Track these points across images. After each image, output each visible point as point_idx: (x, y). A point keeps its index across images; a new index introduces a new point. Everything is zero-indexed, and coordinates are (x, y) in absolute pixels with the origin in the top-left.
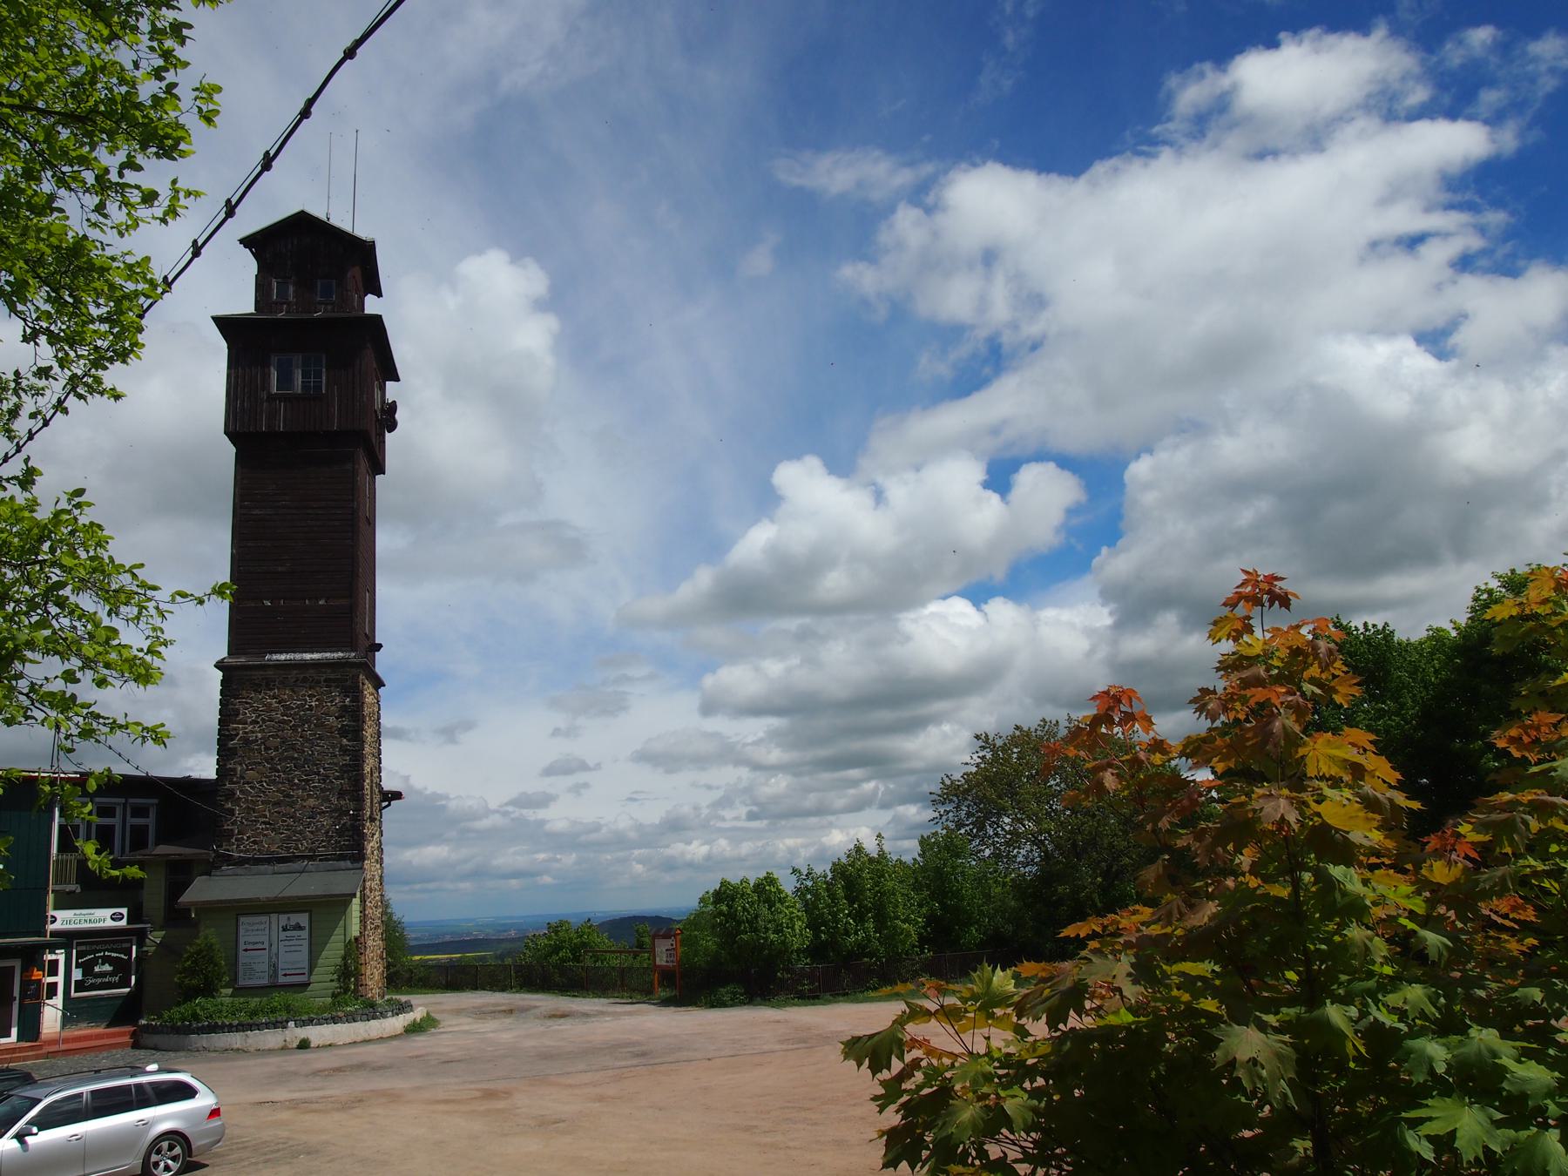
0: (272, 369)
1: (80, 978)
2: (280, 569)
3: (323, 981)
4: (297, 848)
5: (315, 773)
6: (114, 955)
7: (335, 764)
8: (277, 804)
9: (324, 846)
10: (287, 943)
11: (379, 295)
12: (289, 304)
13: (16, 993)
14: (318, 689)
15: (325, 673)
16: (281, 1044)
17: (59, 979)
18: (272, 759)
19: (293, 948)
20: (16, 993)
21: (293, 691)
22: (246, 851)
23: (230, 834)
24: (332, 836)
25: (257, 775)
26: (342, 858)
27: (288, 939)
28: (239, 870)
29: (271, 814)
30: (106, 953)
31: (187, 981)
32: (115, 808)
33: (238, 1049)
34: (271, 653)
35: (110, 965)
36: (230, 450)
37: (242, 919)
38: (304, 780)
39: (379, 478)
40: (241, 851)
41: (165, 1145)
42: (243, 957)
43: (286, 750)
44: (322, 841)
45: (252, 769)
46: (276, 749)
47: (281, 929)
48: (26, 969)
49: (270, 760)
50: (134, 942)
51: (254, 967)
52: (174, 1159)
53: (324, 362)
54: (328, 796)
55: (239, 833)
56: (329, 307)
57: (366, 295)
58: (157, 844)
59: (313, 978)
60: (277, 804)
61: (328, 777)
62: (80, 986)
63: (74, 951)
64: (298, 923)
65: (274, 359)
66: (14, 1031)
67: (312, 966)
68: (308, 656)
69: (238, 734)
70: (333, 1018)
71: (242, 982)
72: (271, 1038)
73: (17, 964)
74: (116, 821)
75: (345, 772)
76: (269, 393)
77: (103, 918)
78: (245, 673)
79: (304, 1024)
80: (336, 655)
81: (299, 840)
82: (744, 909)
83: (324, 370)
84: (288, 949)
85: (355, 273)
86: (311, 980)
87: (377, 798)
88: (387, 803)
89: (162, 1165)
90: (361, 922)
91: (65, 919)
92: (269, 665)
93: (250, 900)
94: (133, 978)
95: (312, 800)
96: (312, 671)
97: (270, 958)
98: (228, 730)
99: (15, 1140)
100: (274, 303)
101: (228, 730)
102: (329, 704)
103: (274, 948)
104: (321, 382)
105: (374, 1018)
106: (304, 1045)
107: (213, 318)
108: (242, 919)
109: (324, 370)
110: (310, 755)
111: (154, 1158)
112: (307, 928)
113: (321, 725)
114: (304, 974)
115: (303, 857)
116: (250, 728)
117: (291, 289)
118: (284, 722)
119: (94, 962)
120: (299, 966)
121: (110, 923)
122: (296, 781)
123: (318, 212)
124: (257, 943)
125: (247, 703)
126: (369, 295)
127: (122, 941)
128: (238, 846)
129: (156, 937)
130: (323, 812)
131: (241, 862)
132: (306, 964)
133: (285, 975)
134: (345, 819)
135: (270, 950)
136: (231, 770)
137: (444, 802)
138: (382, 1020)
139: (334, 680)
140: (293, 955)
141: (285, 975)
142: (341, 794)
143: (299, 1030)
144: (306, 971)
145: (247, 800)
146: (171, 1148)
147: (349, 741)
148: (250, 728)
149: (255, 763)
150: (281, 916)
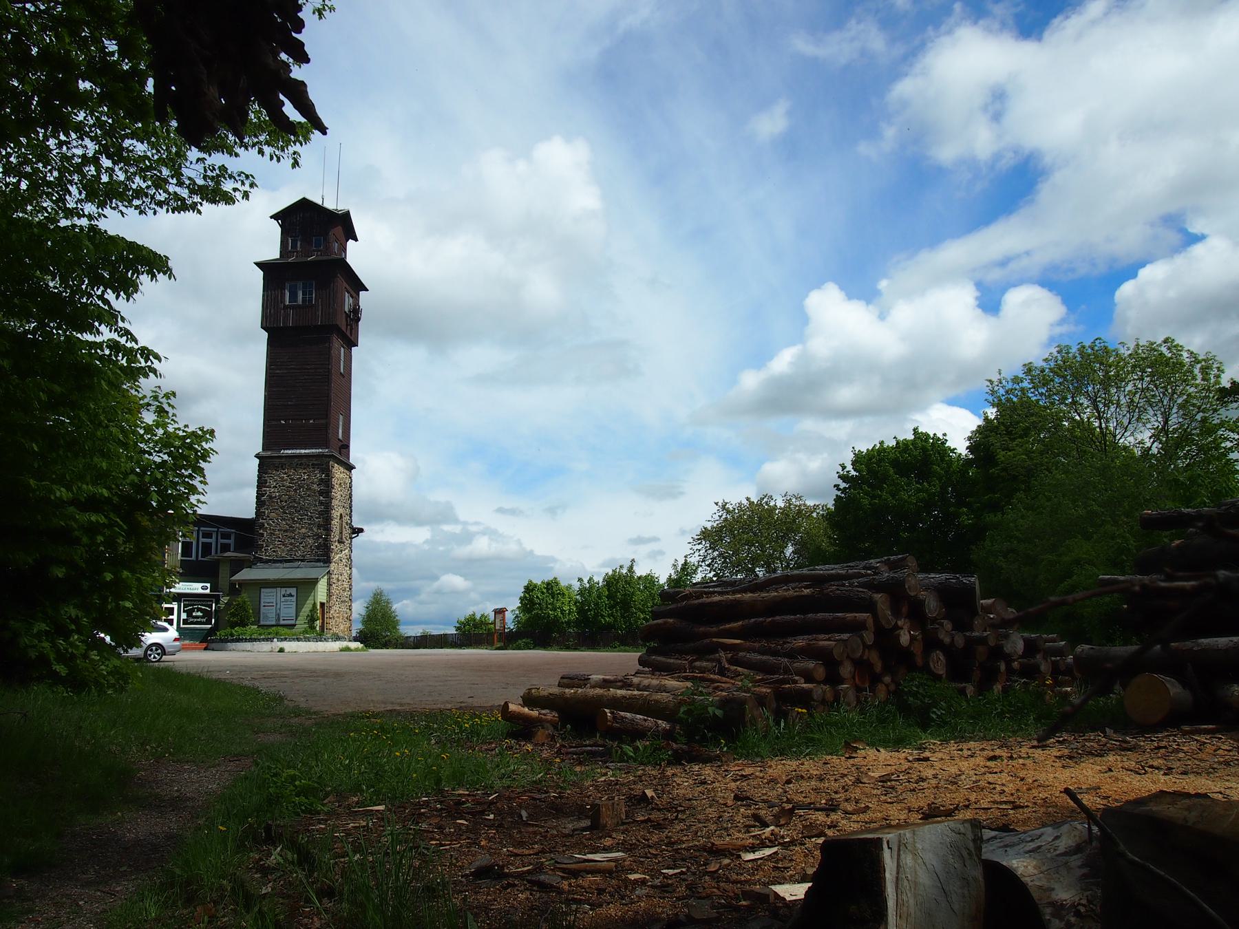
0: (286, 291)
1: (185, 618)
2: (289, 403)
3: (301, 624)
6: (204, 607)
8: (286, 531)
10: (285, 603)
11: (356, 240)
12: (297, 252)
17: (175, 617)
18: (284, 507)
21: (295, 470)
25: (276, 515)
26: (318, 561)
27: (286, 601)
28: (266, 566)
32: (212, 534)
37: (262, 590)
40: (267, 556)
41: (154, 648)
46: (286, 502)
51: (268, 615)
52: (158, 654)
56: (319, 253)
57: (347, 241)
59: (297, 622)
60: (286, 531)
62: (185, 622)
63: (182, 604)
65: (287, 285)
67: (297, 616)
70: (297, 639)
71: (262, 623)
76: (284, 304)
77: (197, 588)
82: (537, 597)
83: (314, 291)
84: (285, 606)
85: (339, 231)
87: (346, 532)
89: (153, 656)
91: (182, 587)
93: (266, 580)
94: (213, 620)
100: (290, 252)
103: (278, 606)
106: (282, 650)
108: (262, 590)
109: (314, 291)
111: (149, 652)
113: (309, 489)
115: (299, 560)
118: (290, 487)
119: (193, 610)
121: (201, 591)
122: (296, 519)
127: (208, 601)
129: (225, 600)
131: (267, 561)
132: (294, 615)
134: (321, 540)
137: (552, 565)
139: (316, 465)
140: (288, 611)
142: (319, 527)
143: (279, 643)
144: (294, 618)
145: (270, 529)
146: (156, 650)
149: (275, 509)
150: (282, 589)
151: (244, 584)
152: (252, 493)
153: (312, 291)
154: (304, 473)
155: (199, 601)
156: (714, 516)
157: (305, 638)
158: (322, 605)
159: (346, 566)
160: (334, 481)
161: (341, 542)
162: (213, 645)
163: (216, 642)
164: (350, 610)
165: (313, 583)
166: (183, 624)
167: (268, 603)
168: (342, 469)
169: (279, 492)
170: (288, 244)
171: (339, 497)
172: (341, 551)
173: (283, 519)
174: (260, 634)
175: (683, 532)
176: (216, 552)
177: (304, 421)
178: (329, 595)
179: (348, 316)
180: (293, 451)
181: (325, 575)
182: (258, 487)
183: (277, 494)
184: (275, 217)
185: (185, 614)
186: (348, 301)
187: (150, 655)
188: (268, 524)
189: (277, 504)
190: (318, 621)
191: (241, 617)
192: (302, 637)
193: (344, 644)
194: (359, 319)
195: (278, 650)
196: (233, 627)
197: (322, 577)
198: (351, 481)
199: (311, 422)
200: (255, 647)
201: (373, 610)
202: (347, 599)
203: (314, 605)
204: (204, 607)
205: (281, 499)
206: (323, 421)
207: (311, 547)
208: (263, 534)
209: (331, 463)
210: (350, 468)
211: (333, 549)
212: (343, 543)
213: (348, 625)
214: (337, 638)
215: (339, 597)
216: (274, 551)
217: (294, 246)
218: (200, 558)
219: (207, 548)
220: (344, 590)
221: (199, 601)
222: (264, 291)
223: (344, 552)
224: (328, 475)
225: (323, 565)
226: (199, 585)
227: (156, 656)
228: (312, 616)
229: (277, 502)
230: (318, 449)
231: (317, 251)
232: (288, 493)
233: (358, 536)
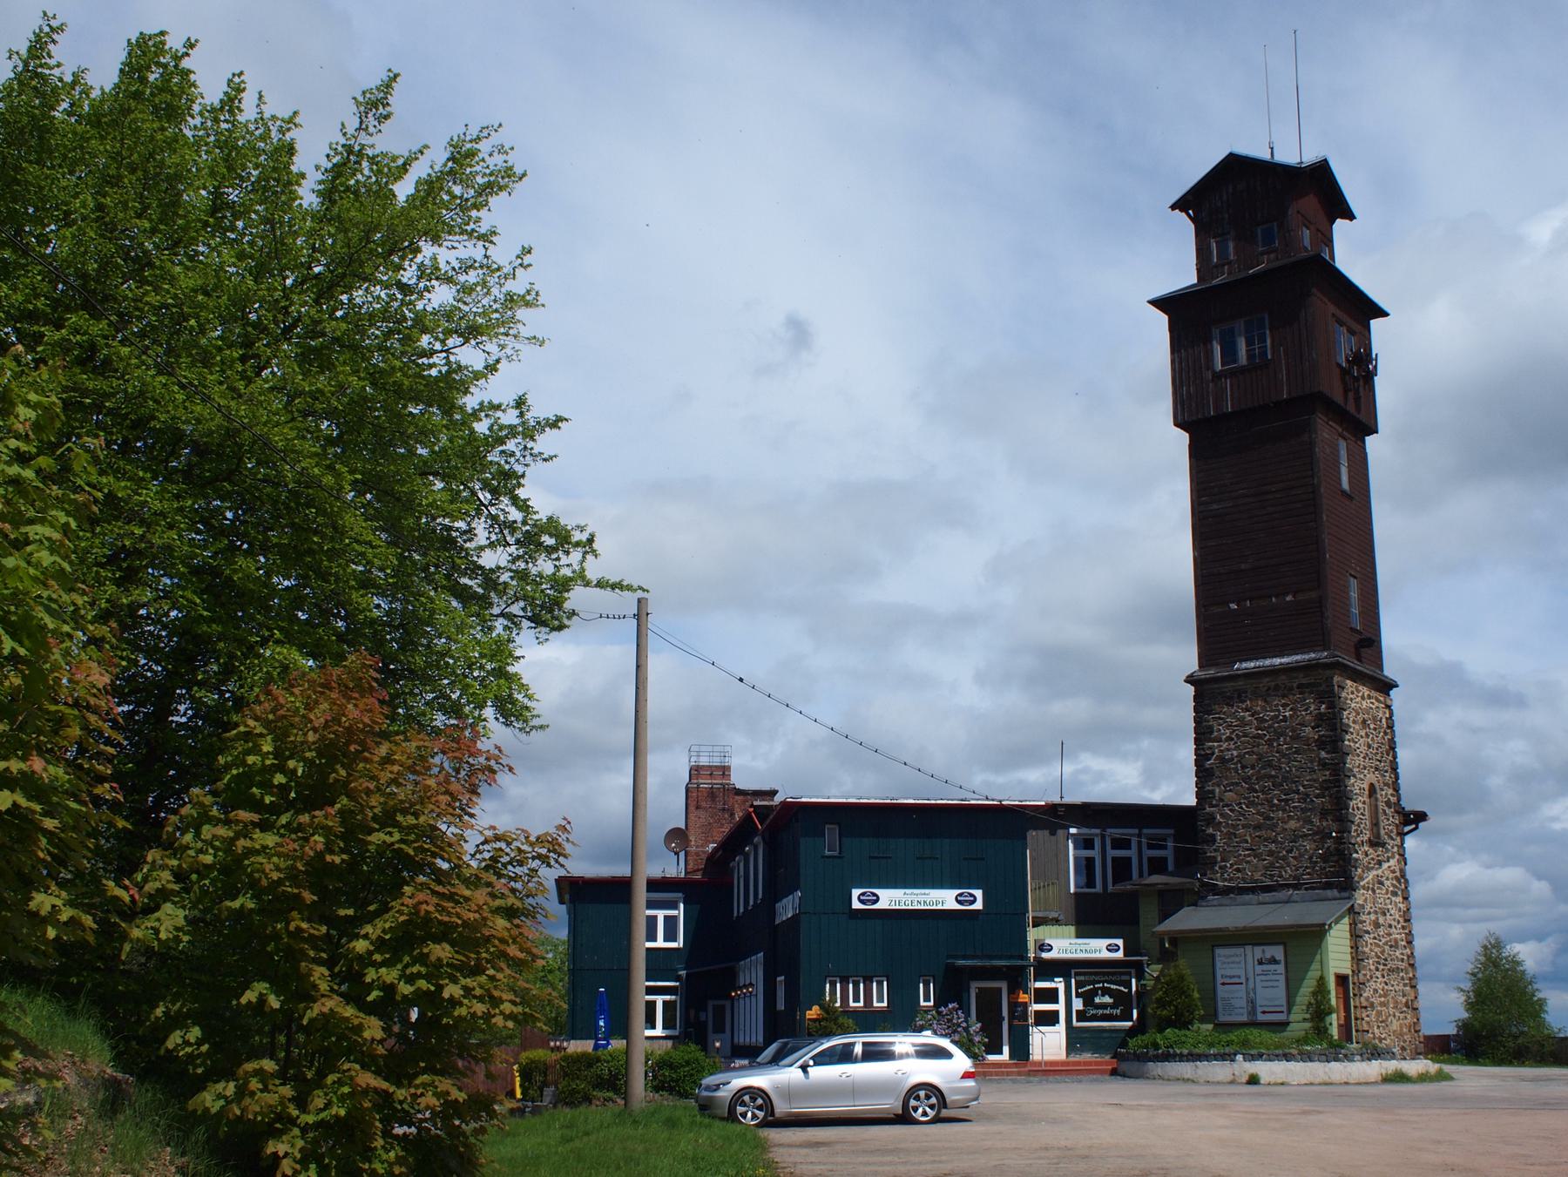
0: (1214, 343)
1: (1081, 1007)
3: (1299, 1024)
4: (1281, 876)
5: (1294, 792)
7: (1315, 781)
8: (1258, 827)
9: (1308, 874)
10: (1263, 978)
11: (1350, 216)
12: (1229, 263)
13: (1005, 1013)
14: (1291, 697)
15: (1296, 678)
16: (1230, 1078)
17: (1060, 1007)
18: (1249, 778)
19: (1270, 984)
20: (1005, 1013)
21: (1266, 701)
22: (1231, 880)
23: (1213, 862)
24: (1316, 862)
25: (1235, 796)
26: (1328, 886)
27: (1265, 973)
28: (1225, 900)
29: (1252, 838)
31: (1158, 1013)
33: (1188, 1080)
34: (1241, 661)
36: (1183, 438)
37: (1219, 951)
38: (1283, 800)
39: (1370, 441)
40: (1225, 880)
42: (1222, 992)
43: (1263, 768)
44: (1307, 867)
45: (1230, 790)
46: (1253, 767)
47: (1256, 962)
48: (1013, 991)
49: (1247, 779)
50: (1133, 974)
51: (1232, 1000)
52: (932, 1107)
53: (1267, 322)
54: (1309, 817)
55: (1223, 860)
58: (1150, 874)
59: (1292, 1017)
60: (1258, 827)
61: (1308, 795)
62: (1082, 1016)
63: (1073, 981)
64: (1273, 957)
65: (1216, 332)
66: (1006, 1049)
67: (1290, 1004)
68: (1277, 661)
69: (1213, 754)
71: (1223, 1018)
72: (1219, 1071)
73: (1004, 986)
74: (1132, 853)
75: (1327, 789)
77: (1098, 948)
78: (1216, 686)
79: (1253, 1058)
80: (1306, 657)
81: (1282, 867)
83: (1268, 332)
84: (1265, 984)
86: (1291, 1020)
87: (1389, 822)
88: (1414, 826)
89: (920, 1110)
90: (1353, 958)
91: (1064, 944)
92: (1239, 676)
93: (1220, 930)
94: (1135, 1012)
95: (1293, 822)
96: (1284, 677)
97: (1248, 993)
98: (1203, 749)
99: (800, 1070)
101: (1203, 749)
103: (1251, 985)
104: (1266, 346)
105: (1337, 1059)
106: (1253, 1080)
107: (1150, 302)
109: (1268, 332)
110: (1288, 772)
111: (913, 1103)
112: (1283, 962)
113: (1296, 738)
114: (1282, 1012)
115: (1288, 886)
116: (1225, 745)
117: (1231, 245)
119: (1094, 993)
120: (1277, 1003)
121: (1106, 955)
122: (1276, 801)
123: (1257, 150)
124: (1234, 977)
125: (1220, 718)
126: (1339, 221)
128: (1222, 875)
130: (1306, 835)
131: (1226, 891)
132: (1283, 1001)
133: (1264, 1012)
134: (1329, 843)
135: (1247, 984)
136: (1209, 791)
138: (1346, 1064)
140: (1271, 993)
141: (1264, 1012)
142: (1324, 814)
144: (1284, 1009)
146: (928, 1097)
147: (1328, 753)
148: (1225, 745)
149: (1233, 784)
150: (1256, 948)
151: (1177, 939)
152: (1186, 753)
153: (1265, 333)
154: (1284, 706)
157: (1301, 1053)
158: (1342, 980)
159: (1395, 894)
160: (1348, 717)
161: (1376, 843)
162: (1125, 1066)
163: (1128, 1060)
164: (1413, 987)
165: (1315, 935)
166: (1077, 1021)
167: (1231, 977)
168: (1365, 691)
170: (1211, 253)
171: (1363, 749)
172: (1380, 863)
173: (1250, 804)
174: (1211, 1045)
175: (390, 70)
176: (1141, 875)
177: (1274, 599)
178: (1358, 958)
179: (1345, 372)
180: (1259, 663)
181: (1341, 917)
182: (1197, 741)
183: (1235, 753)
184: (1181, 205)
186: (1344, 347)
187: (915, 1109)
188: (1221, 815)
189: (1237, 772)
190: (1334, 1016)
191: (1176, 1007)
192: (1294, 1052)
193: (1391, 1066)
194: (1374, 372)
195: (1244, 1079)
196: (1161, 1030)
197: (1337, 922)
198: (1391, 714)
199: (1289, 598)
200: (1200, 1072)
201: (1487, 981)
202: (1403, 965)
203: (1322, 981)
206: (1313, 595)
207: (1311, 858)
208: (1213, 837)
209: (1336, 679)
210: (1386, 686)
211: (1357, 860)
212: (1383, 845)
213: (1410, 1019)
214: (1374, 1053)
215: (1382, 961)
216: (1238, 870)
217: (1222, 252)
218: (1110, 887)
219: (1122, 869)
220: (1395, 946)
222: (1173, 351)
223: (1385, 866)
224: (1331, 706)
226: (1102, 943)
227: (928, 1109)
228: (1318, 1004)
229: (1236, 770)
230: (1308, 652)
232: (1255, 749)
233: (1416, 828)
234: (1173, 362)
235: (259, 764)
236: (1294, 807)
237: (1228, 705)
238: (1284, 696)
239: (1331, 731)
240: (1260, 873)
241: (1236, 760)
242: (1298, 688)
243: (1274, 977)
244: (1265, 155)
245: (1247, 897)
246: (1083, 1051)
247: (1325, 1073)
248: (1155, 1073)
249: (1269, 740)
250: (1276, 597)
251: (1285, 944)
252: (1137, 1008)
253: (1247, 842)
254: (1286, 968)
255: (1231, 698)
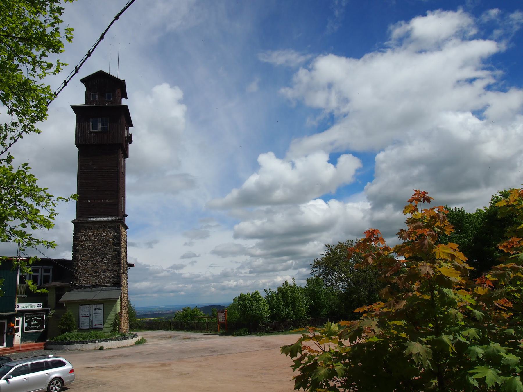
0: (91, 123)
2: (93, 190)
3: (108, 327)
5: (105, 258)
6: (38, 318)
8: (93, 268)
9: (108, 282)
10: (96, 314)
11: (127, 98)
12: (96, 101)
13: (5, 331)
14: (106, 230)
16: (94, 348)
17: (20, 326)
18: (91, 253)
19: (98, 316)
20: (5, 331)
21: (98, 230)
22: (82, 284)
26: (114, 286)
27: (96, 313)
28: (80, 290)
30: (35, 318)
32: (38, 269)
33: (79, 350)
35: (37, 322)
36: (77, 150)
37: (81, 306)
38: (101, 260)
40: (81, 284)
41: (55, 382)
42: (81, 319)
43: (95, 250)
45: (84, 256)
46: (92, 250)
47: (94, 310)
48: (9, 323)
49: (90, 253)
51: (85, 322)
52: (58, 386)
58: (52, 281)
59: (104, 326)
60: (93, 268)
62: (27, 329)
63: (25, 317)
65: (92, 120)
66: (5, 344)
68: (103, 219)
69: (79, 245)
71: (81, 328)
72: (90, 346)
73: (6, 321)
74: (39, 274)
77: (34, 306)
79: (101, 341)
80: (112, 218)
83: (108, 123)
85: (118, 91)
87: (126, 266)
91: (22, 306)
95: (104, 267)
97: (90, 319)
98: (76, 243)
99: (5, 380)
101: (76, 243)
102: (110, 235)
105: (125, 339)
106: (101, 348)
107: (71, 106)
110: (103, 252)
111: (51, 386)
112: (102, 309)
113: (107, 242)
114: (101, 325)
115: (101, 286)
118: (95, 241)
119: (31, 321)
121: (37, 308)
122: (99, 260)
124: (86, 314)
125: (82, 234)
126: (123, 98)
127: (41, 314)
128: (79, 282)
129: (52, 312)
130: (108, 271)
131: (80, 287)
132: (102, 322)
133: (95, 325)
134: (115, 273)
135: (90, 317)
137: (148, 268)
138: (127, 340)
140: (98, 318)
141: (95, 325)
142: (114, 265)
144: (102, 324)
145: (82, 267)
146: (57, 383)
147: (116, 247)
149: (85, 254)
155: (35, 314)
156: (325, 252)
165: (115, 300)
167: (85, 314)
169: (87, 244)
180: (97, 219)
185: (27, 324)
187: (52, 388)
189: (87, 251)
200: (83, 347)
204: (38, 318)
205: (89, 248)
207: (109, 277)
217: (94, 97)
221: (35, 314)
225: (117, 289)
230: (112, 217)
231: (109, 101)
232: (93, 244)
233: (130, 268)
234: (76, 125)
235: (519, 377)
236: (104, 262)
237: (85, 230)
238: (104, 229)
239: (118, 240)
240: (92, 282)
241: (87, 247)
242: (108, 227)
243: (100, 314)
244: (108, 72)
245: (87, 289)
246: (26, 341)
247: (122, 344)
248: (66, 348)
249: (98, 242)
250: (103, 200)
251: (104, 304)
252: (45, 325)
253: (88, 272)
254: (104, 312)
255: (86, 228)
